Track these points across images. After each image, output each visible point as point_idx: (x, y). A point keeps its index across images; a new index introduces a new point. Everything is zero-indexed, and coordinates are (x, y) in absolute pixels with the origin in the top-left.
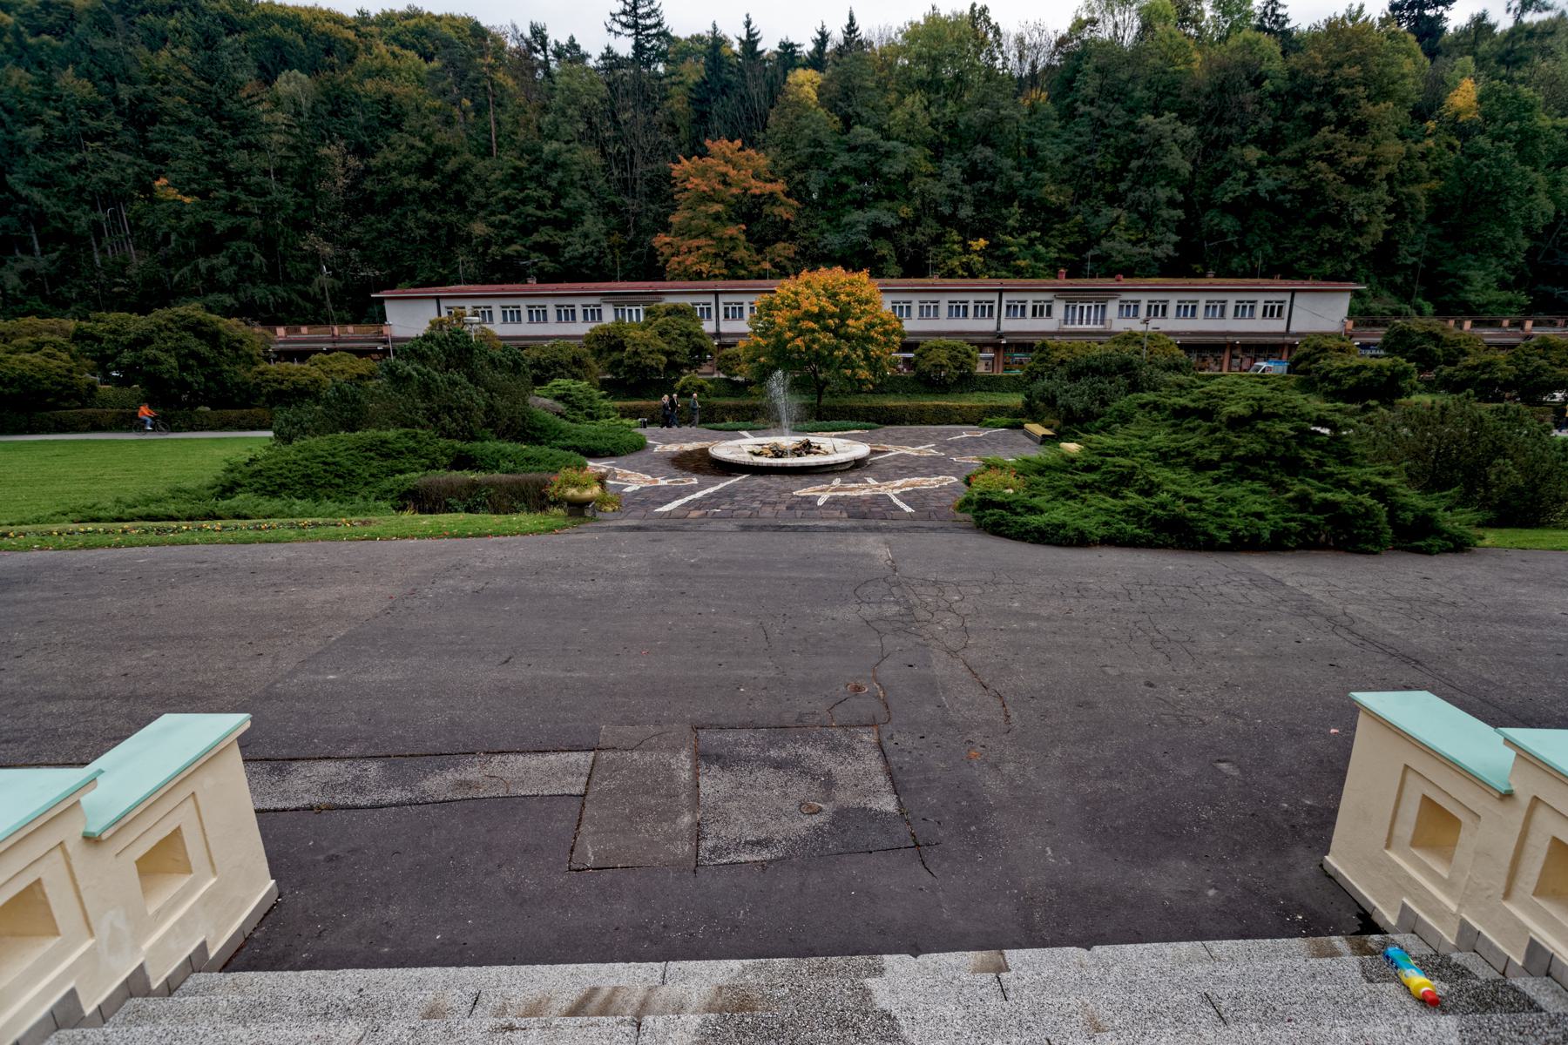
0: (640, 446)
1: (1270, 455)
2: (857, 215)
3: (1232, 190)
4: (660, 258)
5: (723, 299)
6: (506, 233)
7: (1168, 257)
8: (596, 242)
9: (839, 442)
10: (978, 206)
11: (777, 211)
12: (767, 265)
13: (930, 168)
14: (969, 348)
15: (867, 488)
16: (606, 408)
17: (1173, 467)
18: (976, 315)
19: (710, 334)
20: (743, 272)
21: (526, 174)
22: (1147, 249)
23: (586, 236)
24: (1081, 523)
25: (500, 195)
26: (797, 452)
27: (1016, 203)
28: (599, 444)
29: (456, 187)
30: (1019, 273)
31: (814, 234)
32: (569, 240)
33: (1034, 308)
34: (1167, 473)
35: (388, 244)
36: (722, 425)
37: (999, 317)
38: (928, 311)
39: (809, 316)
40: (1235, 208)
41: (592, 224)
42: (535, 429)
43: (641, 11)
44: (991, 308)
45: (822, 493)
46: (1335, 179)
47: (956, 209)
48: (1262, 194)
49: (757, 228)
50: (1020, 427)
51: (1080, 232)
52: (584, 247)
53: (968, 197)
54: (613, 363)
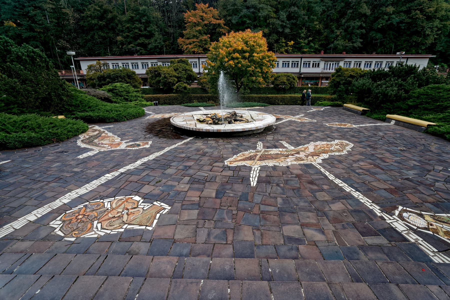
3: (381, 23)
4: (180, 46)
5: (201, 60)
6: (129, 40)
7: (359, 47)
10: (291, 29)
11: (221, 30)
18: (292, 67)
19: (197, 73)
21: (135, 19)
25: (126, 26)
29: (112, 24)
30: (304, 53)
33: (313, 64)
35: (89, 44)
36: (191, 104)
37: (300, 67)
39: (235, 51)
40: (381, 31)
44: (298, 64)
46: (422, 17)
47: (284, 29)
51: (325, 40)
54: (157, 81)
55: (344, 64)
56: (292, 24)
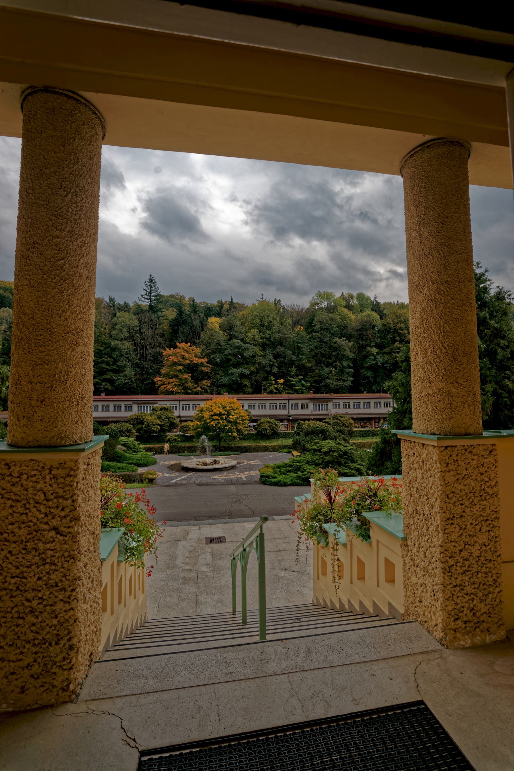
0: (154, 463)
1: (333, 461)
2: (234, 370)
3: (368, 363)
4: (156, 386)
7: (349, 386)
8: (130, 379)
9: (226, 460)
10: (279, 367)
11: (203, 369)
12: (199, 389)
13: (261, 353)
14: (276, 422)
15: (233, 475)
16: (140, 448)
17: (311, 465)
18: (280, 408)
20: (190, 391)
21: (104, 352)
22: (342, 383)
23: (126, 376)
24: (285, 480)
26: (212, 464)
27: (294, 367)
28: (141, 462)
30: (297, 392)
31: (218, 377)
32: (119, 377)
33: (302, 405)
34: (309, 467)
36: (184, 454)
37: (179, 409)
38: (263, 407)
40: (371, 368)
41: (129, 372)
42: (117, 457)
43: (152, 294)
44: (285, 405)
45: (220, 477)
48: (379, 364)
49: (196, 374)
50: (290, 452)
52: (125, 380)
53: (276, 364)
55: (333, 405)
56: (280, 362)
